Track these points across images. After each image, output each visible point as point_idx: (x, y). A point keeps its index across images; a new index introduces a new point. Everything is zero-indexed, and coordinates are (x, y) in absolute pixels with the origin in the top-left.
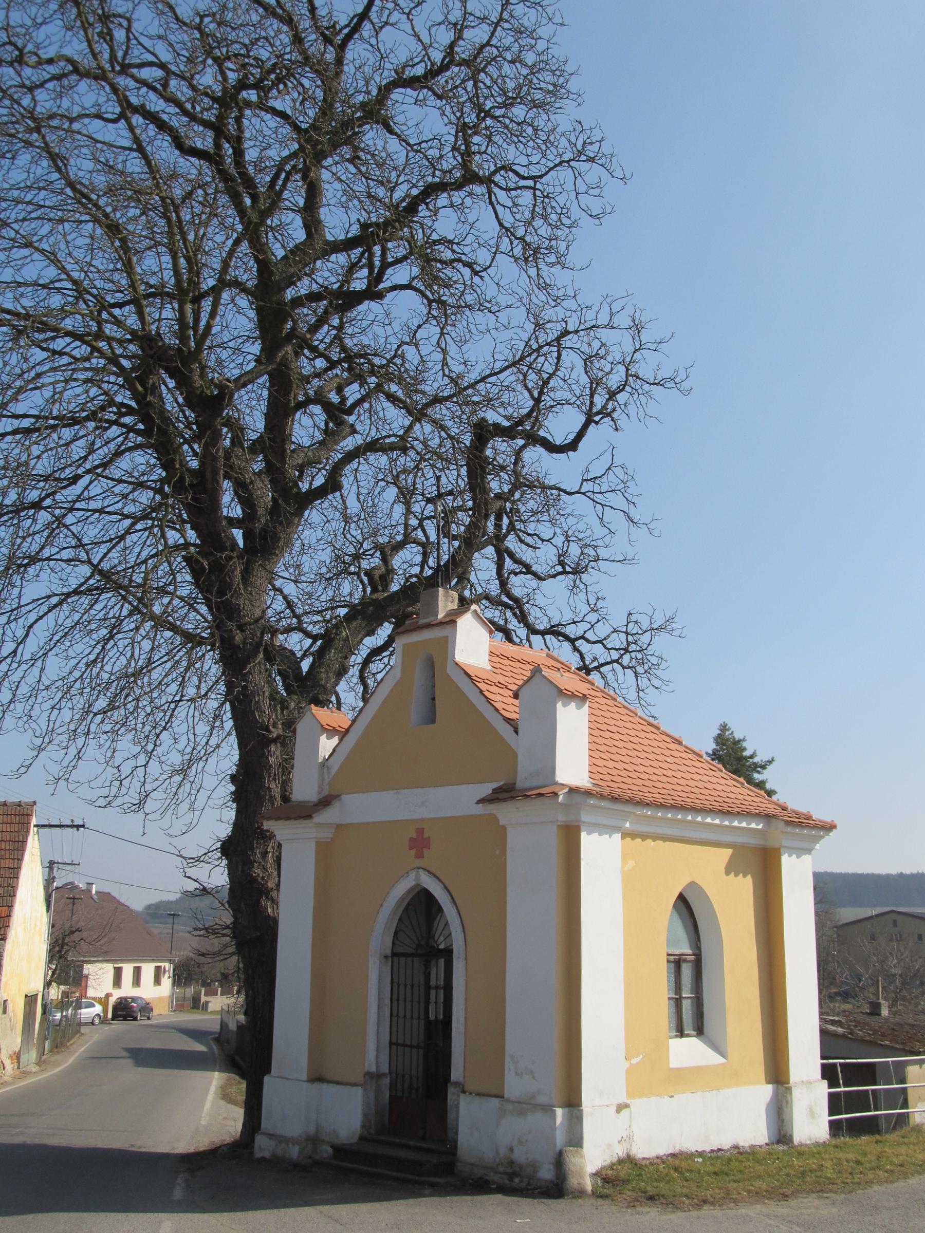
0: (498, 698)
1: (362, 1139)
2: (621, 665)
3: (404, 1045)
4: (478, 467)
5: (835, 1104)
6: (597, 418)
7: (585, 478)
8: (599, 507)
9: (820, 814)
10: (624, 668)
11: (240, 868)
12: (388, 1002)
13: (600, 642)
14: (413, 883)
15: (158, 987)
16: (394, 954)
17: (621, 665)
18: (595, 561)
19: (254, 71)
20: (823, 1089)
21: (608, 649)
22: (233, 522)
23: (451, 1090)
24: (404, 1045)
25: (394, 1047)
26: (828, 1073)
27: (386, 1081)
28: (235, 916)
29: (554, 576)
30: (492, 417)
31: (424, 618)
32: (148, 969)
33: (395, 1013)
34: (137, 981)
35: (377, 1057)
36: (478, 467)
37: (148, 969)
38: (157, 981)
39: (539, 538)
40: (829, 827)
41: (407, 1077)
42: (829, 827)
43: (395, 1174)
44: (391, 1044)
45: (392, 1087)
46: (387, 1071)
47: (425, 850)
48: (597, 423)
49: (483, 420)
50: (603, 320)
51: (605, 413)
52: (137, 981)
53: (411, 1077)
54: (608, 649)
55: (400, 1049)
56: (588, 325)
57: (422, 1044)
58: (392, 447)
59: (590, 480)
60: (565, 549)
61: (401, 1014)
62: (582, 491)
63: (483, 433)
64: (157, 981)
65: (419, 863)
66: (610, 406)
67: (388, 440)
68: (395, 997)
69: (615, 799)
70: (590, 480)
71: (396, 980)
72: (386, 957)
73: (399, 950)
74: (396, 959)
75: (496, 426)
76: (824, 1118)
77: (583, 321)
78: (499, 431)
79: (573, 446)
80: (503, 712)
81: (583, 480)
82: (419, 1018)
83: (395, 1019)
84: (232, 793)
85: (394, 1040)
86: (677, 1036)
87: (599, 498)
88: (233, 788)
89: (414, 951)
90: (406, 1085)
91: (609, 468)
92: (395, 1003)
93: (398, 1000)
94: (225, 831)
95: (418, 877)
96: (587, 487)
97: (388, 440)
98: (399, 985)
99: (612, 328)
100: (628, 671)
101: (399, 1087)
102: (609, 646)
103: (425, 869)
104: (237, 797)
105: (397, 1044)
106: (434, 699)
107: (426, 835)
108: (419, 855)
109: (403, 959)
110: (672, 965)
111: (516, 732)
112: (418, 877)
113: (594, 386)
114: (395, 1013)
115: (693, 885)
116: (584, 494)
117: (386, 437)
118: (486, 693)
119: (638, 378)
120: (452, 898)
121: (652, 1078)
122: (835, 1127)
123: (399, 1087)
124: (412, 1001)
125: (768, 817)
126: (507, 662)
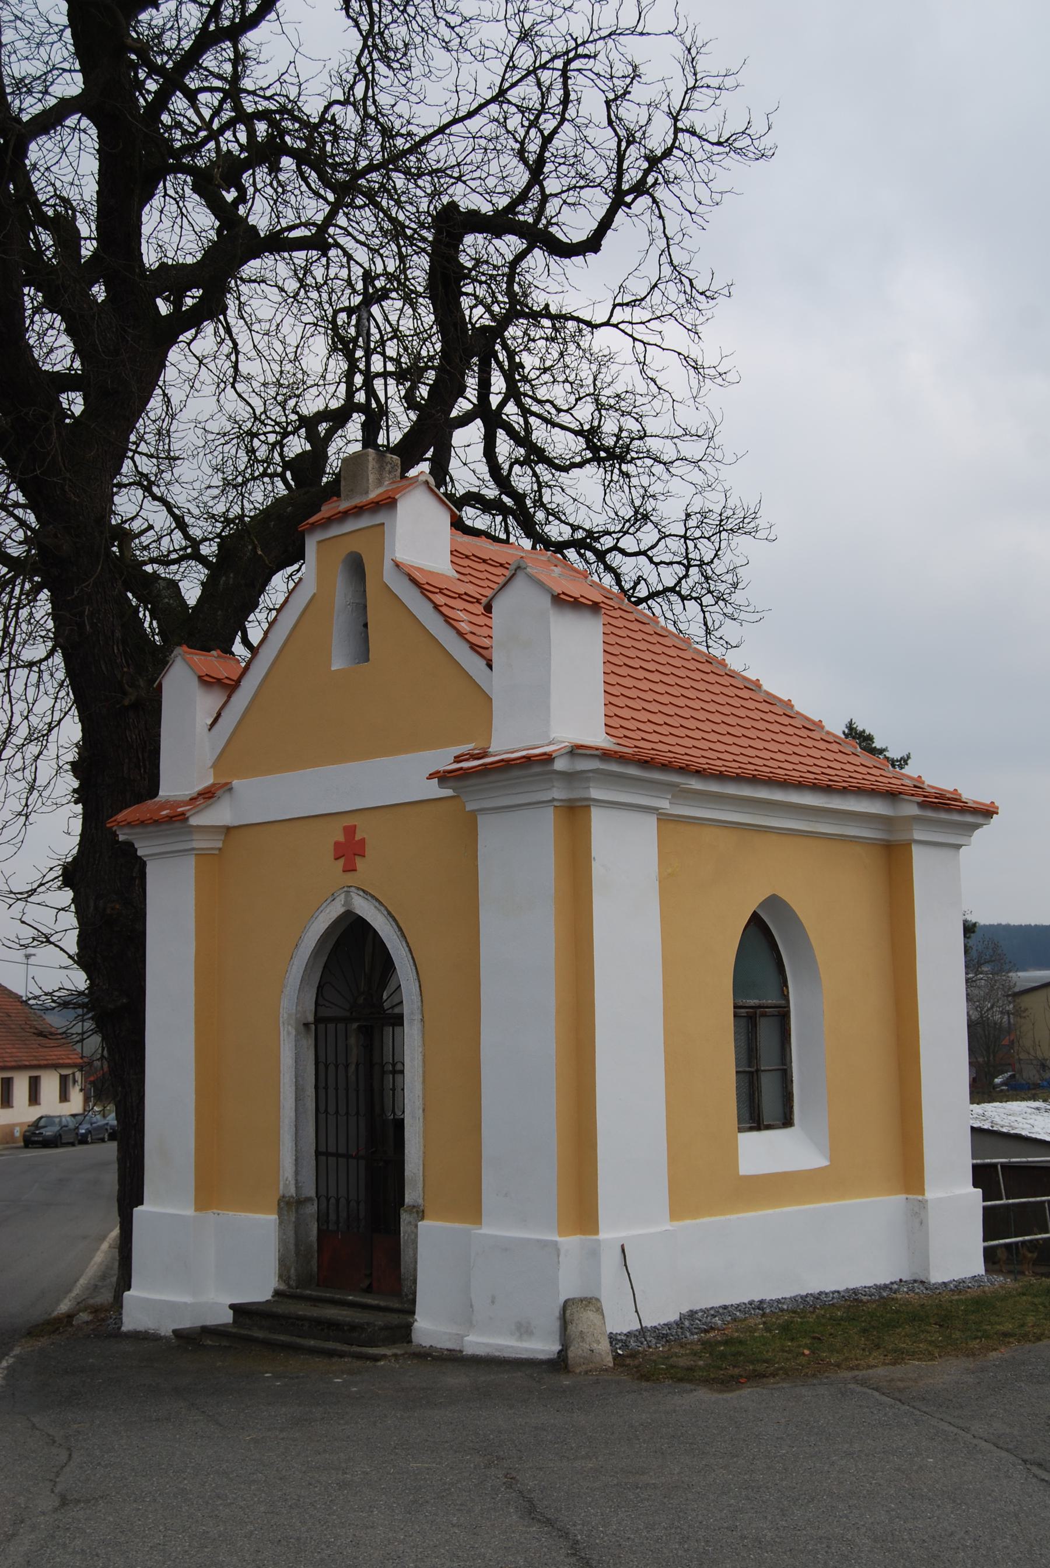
0: (462, 615)
1: (277, 1293)
2: (679, 594)
3: (337, 1155)
4: (446, 282)
5: (994, 1223)
6: (628, 199)
7: (618, 300)
8: (639, 346)
9: (972, 793)
10: (683, 598)
11: (92, 904)
12: (310, 1091)
13: (644, 553)
14: (341, 910)
15: (66, 1104)
16: (318, 1020)
17: (679, 594)
18: (641, 438)
19: (428, 185)
20: (971, 1199)
21: (657, 564)
22: (65, 381)
23: (405, 1217)
24: (337, 1155)
25: (323, 1158)
26: (982, 1176)
27: (312, 1209)
28: (90, 978)
29: (580, 465)
30: (469, 200)
31: (348, 497)
32: (50, 1084)
33: (322, 1109)
34: (34, 1098)
35: (297, 1173)
36: (446, 282)
37: (50, 1084)
38: (64, 1097)
39: (554, 406)
40: (987, 812)
41: (343, 1201)
42: (987, 812)
43: (283, 1338)
44: (318, 1153)
45: (322, 1218)
46: (312, 1193)
47: (358, 860)
48: (629, 206)
49: (453, 206)
50: (628, 20)
51: (640, 189)
52: (34, 1098)
53: (348, 1202)
54: (657, 564)
55: (332, 1160)
56: (604, 33)
57: (362, 1153)
58: (301, 244)
59: (627, 304)
60: (596, 423)
61: (332, 1109)
62: (614, 321)
63: (452, 224)
64: (64, 1097)
65: (350, 879)
66: (650, 180)
67: (294, 234)
68: (322, 1084)
69: (646, 763)
70: (627, 304)
71: (322, 1059)
72: (306, 1025)
73: (325, 1012)
74: (321, 1026)
75: (474, 214)
76: (977, 1245)
77: (595, 27)
78: (476, 222)
79: (592, 244)
80: (469, 637)
81: (615, 306)
82: (358, 1113)
83: (322, 1116)
84: (75, 791)
85: (323, 1149)
86: (751, 1129)
87: (640, 331)
88: (76, 784)
89: (348, 1014)
90: (343, 1215)
91: (656, 285)
92: (322, 1093)
93: (326, 1088)
94: (69, 846)
95: (348, 902)
96: (619, 315)
97: (294, 234)
98: (327, 1067)
99: (642, 34)
100: (691, 605)
101: (332, 1217)
102: (656, 559)
103: (358, 889)
104: (82, 795)
105: (327, 1154)
106: (366, 625)
107: (358, 837)
108: (350, 868)
109: (331, 1026)
110: (743, 1022)
111: (490, 666)
112: (348, 902)
113: (624, 144)
114: (322, 1109)
115: (774, 902)
116: (616, 326)
117: (291, 228)
118: (444, 609)
119: (693, 133)
120: (400, 929)
121: (700, 1185)
122: (989, 1255)
123: (332, 1217)
124: (337, 1089)
125: (892, 795)
126: (482, 567)
